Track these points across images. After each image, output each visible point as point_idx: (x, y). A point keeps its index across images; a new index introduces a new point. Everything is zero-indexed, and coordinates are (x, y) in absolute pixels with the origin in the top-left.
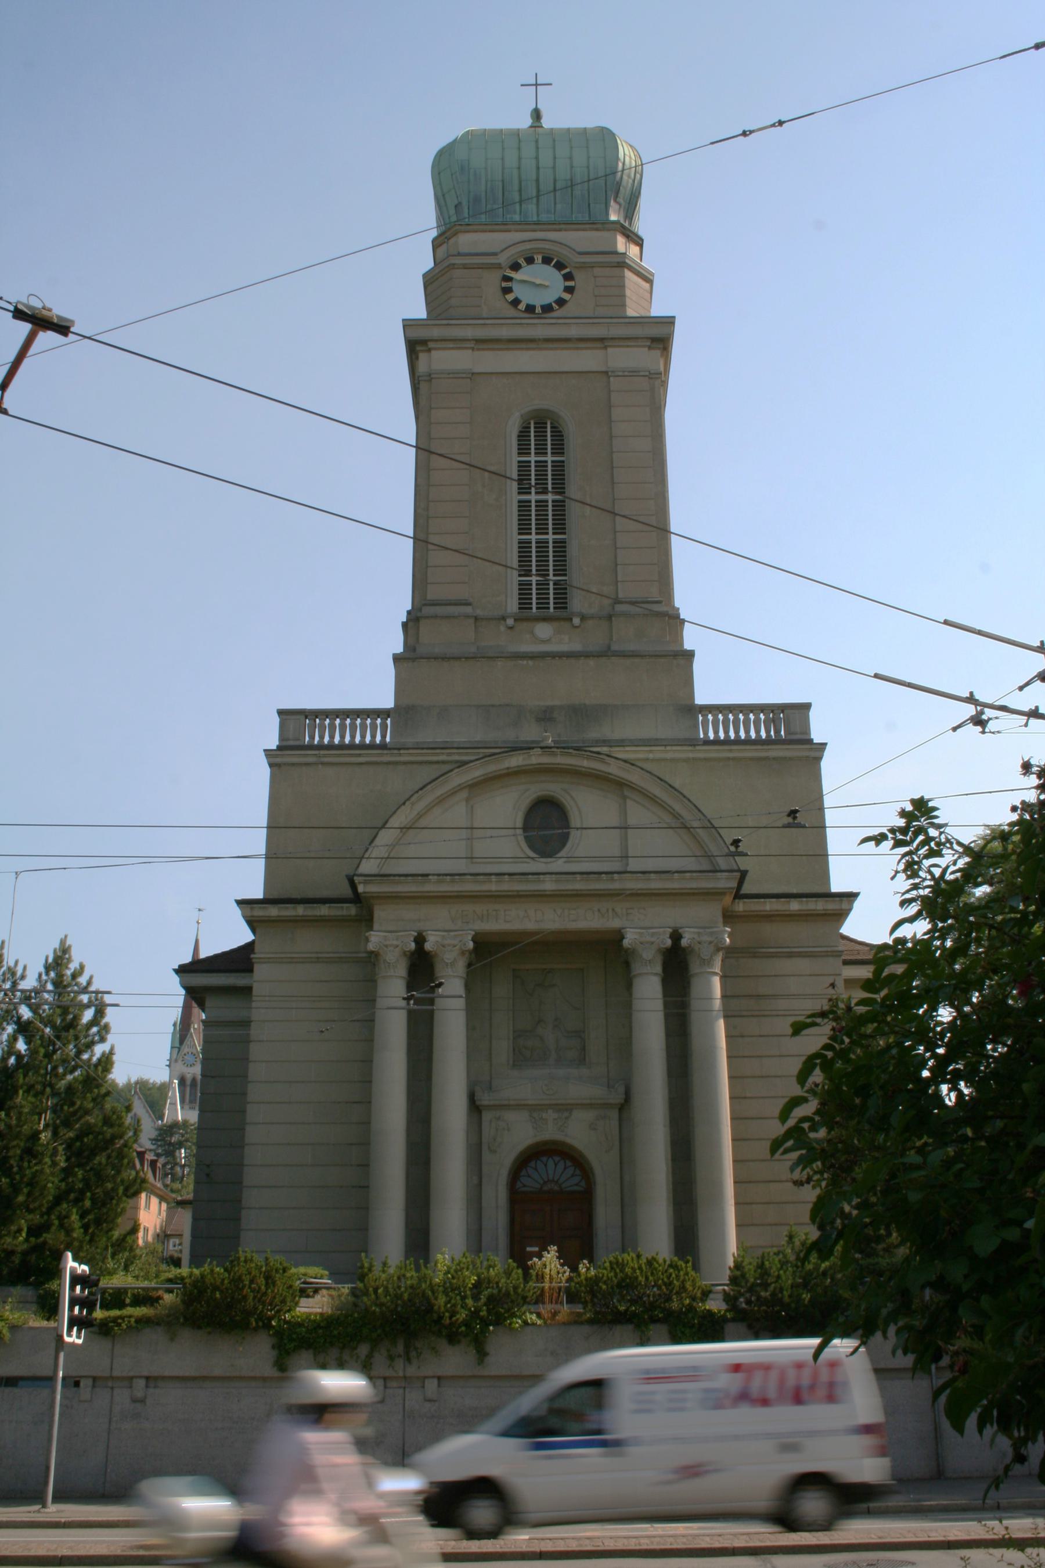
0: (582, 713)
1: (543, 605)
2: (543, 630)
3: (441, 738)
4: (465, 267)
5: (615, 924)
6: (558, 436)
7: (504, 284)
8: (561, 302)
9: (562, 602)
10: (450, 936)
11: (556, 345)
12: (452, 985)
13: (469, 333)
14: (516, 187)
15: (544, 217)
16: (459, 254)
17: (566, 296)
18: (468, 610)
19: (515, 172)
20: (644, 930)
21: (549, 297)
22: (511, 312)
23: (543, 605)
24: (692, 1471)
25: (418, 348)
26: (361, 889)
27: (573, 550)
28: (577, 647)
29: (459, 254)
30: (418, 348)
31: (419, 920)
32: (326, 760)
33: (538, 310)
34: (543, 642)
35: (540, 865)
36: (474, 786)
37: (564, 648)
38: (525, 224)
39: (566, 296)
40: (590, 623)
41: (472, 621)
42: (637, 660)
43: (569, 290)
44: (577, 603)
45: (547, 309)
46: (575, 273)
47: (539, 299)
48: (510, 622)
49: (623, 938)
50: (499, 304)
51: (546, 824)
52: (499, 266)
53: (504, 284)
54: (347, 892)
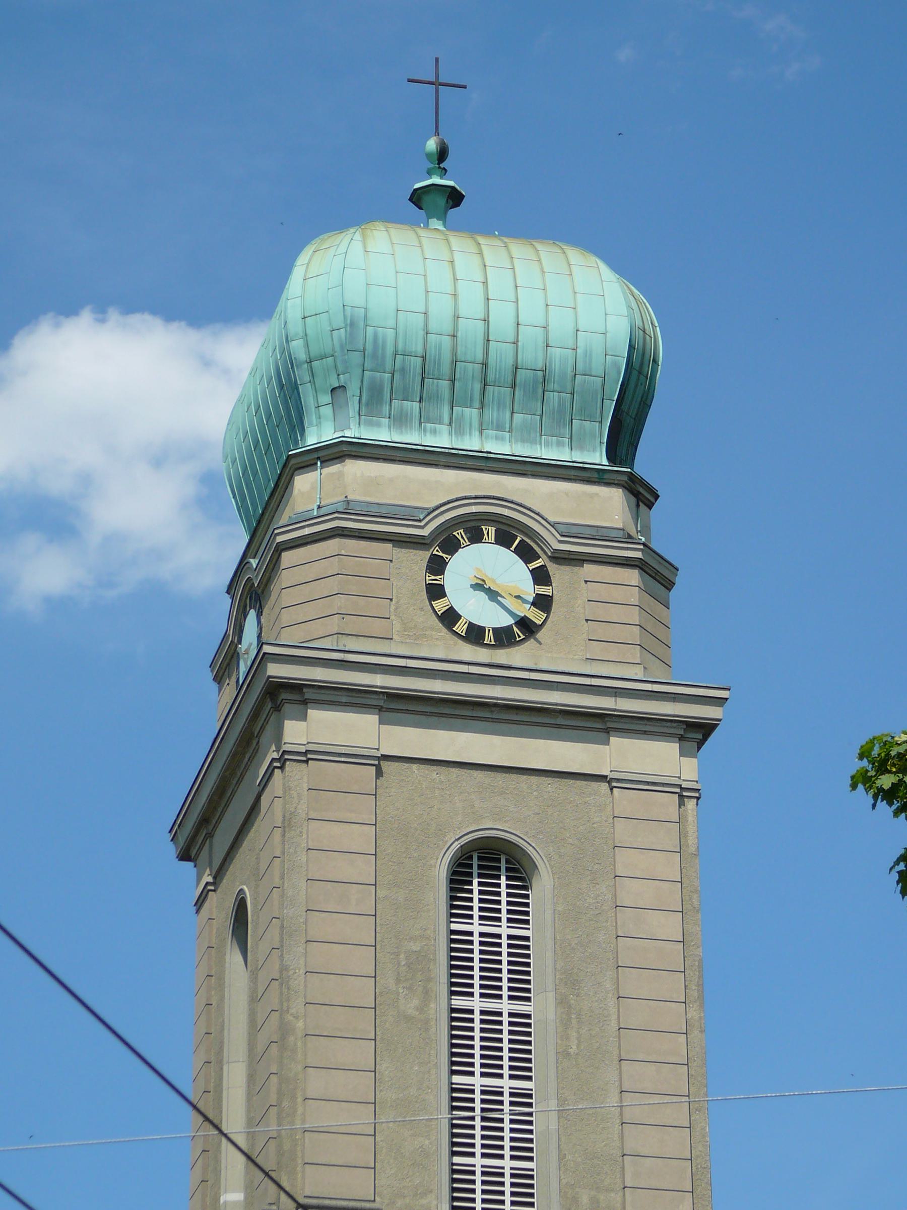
8: (527, 627)
19: (447, 341)
30: (284, 696)
33: (489, 638)
39: (536, 616)
47: (493, 617)
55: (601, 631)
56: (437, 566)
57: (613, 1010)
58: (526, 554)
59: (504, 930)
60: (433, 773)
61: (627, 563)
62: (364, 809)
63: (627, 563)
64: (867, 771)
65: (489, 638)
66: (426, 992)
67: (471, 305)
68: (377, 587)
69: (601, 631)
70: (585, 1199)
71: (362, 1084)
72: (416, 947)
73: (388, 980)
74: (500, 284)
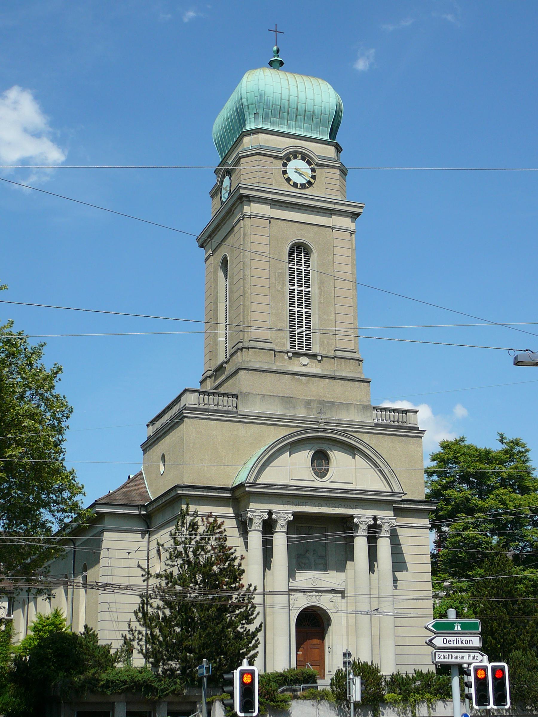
33: (299, 186)
42: (347, 382)
51: (321, 460)
56: (285, 165)
60: (285, 223)
65: (299, 186)
66: (283, 284)
74: (301, 87)
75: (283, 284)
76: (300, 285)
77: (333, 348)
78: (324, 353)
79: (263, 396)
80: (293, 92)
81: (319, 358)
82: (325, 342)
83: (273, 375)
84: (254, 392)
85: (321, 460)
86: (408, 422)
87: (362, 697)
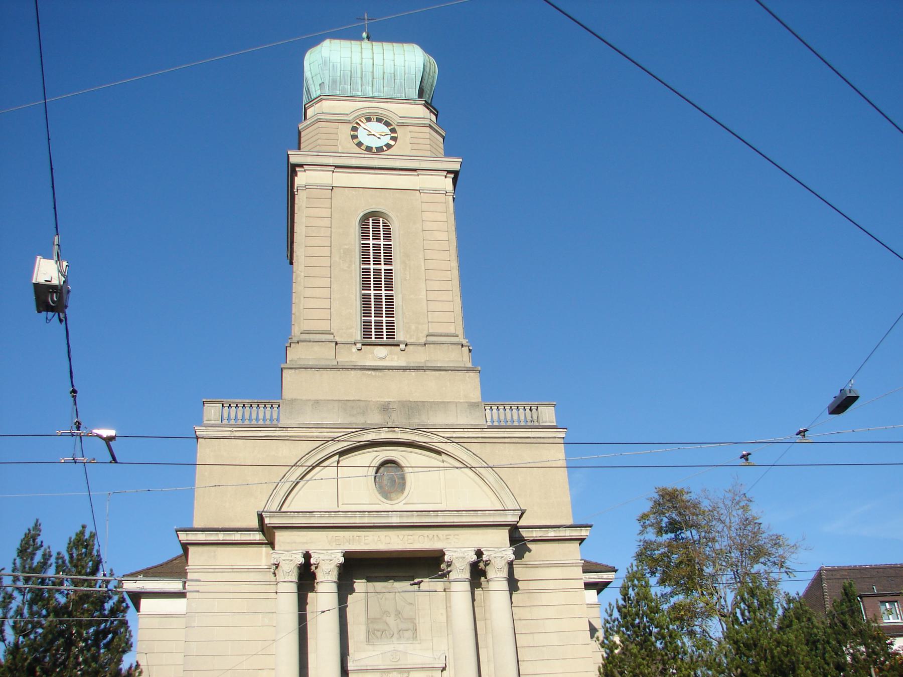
0: (412, 407)
1: (379, 335)
2: (381, 351)
3: (315, 421)
4: (327, 121)
5: (437, 546)
6: (387, 228)
7: (352, 133)
8: (389, 146)
9: (391, 335)
10: (328, 556)
11: (377, 171)
12: (325, 595)
13: (331, 161)
14: (359, 75)
15: (376, 94)
16: (323, 113)
17: (392, 143)
18: (330, 337)
19: (359, 67)
20: (459, 549)
21: (382, 143)
22: (357, 150)
23: (379, 335)
24: (593, 630)
25: (297, 169)
26: (267, 521)
27: (397, 302)
28: (403, 363)
29: (323, 113)
30: (297, 169)
31: (306, 543)
32: (237, 434)
33: (374, 150)
34: (381, 359)
35: (386, 506)
36: (342, 453)
37: (395, 364)
38: (364, 98)
39: (392, 143)
40: (410, 348)
41: (334, 344)
42: (443, 373)
43: (394, 139)
44: (399, 336)
45: (380, 150)
46: (397, 128)
47: (374, 143)
48: (359, 346)
49: (444, 554)
50: (352, 147)
51: (390, 476)
52: (348, 122)
53: (352, 133)
54: (255, 524)
55: (416, 147)
56: (355, 129)
57: (423, 264)
58: (387, 124)
59: (383, 267)
60: (353, 192)
61: (424, 126)
62: (327, 203)
63: (424, 126)
64: (647, 545)
65: (374, 150)
66: (351, 261)
67: (367, 63)
68: (333, 136)
69: (416, 147)
70: (413, 327)
71: (326, 262)
72: (346, 247)
73: (336, 258)
74: (378, 60)
75: (351, 261)
76: (377, 247)
77: (426, 333)
78: (408, 341)
79: (317, 402)
80: (367, 63)
81: (402, 346)
82: (413, 327)
83: (329, 371)
84: (304, 398)
85: (390, 476)
86: (540, 420)
87: (36, 258)
